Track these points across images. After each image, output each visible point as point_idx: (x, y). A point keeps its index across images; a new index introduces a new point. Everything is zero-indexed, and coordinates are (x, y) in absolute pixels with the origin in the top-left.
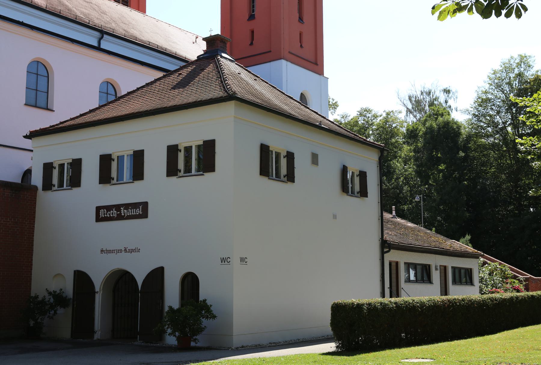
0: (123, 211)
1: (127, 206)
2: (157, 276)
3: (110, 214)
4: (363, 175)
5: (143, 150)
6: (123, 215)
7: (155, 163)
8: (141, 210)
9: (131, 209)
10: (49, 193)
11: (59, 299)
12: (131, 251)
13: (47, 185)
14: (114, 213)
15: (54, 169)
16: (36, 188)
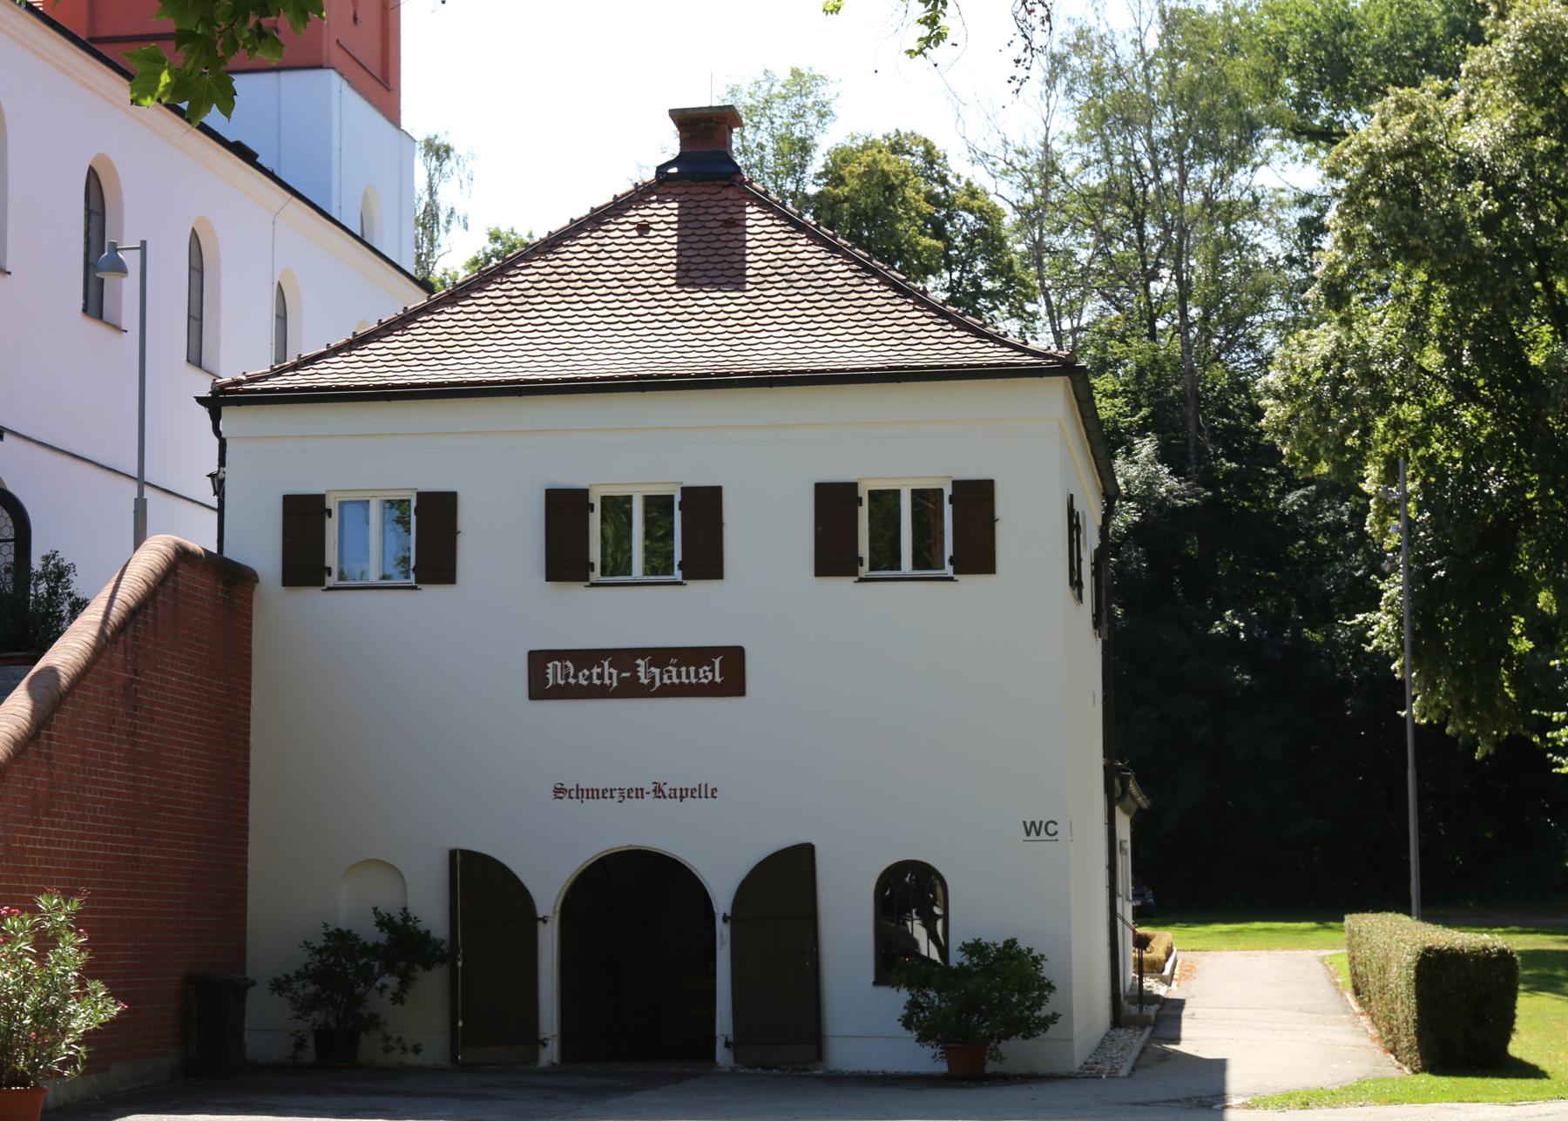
1: (659, 656)
3: (590, 678)
5: (720, 489)
7: (769, 533)
8: (723, 672)
9: (678, 666)
10: (311, 597)
11: (404, 943)
12: (682, 794)
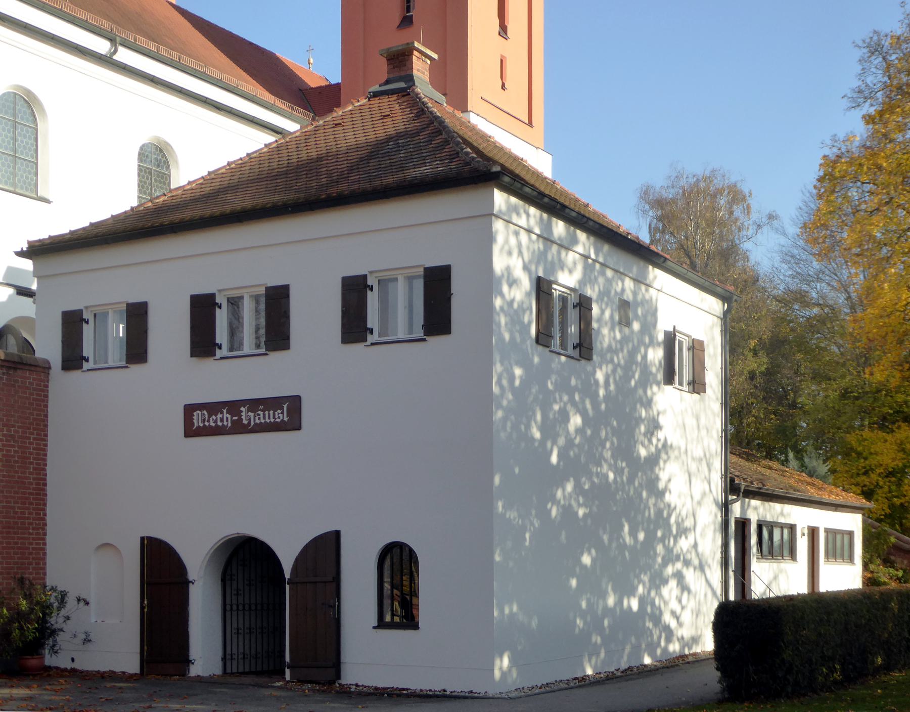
0: (246, 415)
1: (255, 404)
2: (325, 551)
3: (216, 421)
4: (697, 348)
6: (245, 422)
7: (316, 314)
9: (263, 411)
10: (75, 375)
13: (73, 359)
14: (225, 418)
15: (85, 325)
16: (44, 368)
